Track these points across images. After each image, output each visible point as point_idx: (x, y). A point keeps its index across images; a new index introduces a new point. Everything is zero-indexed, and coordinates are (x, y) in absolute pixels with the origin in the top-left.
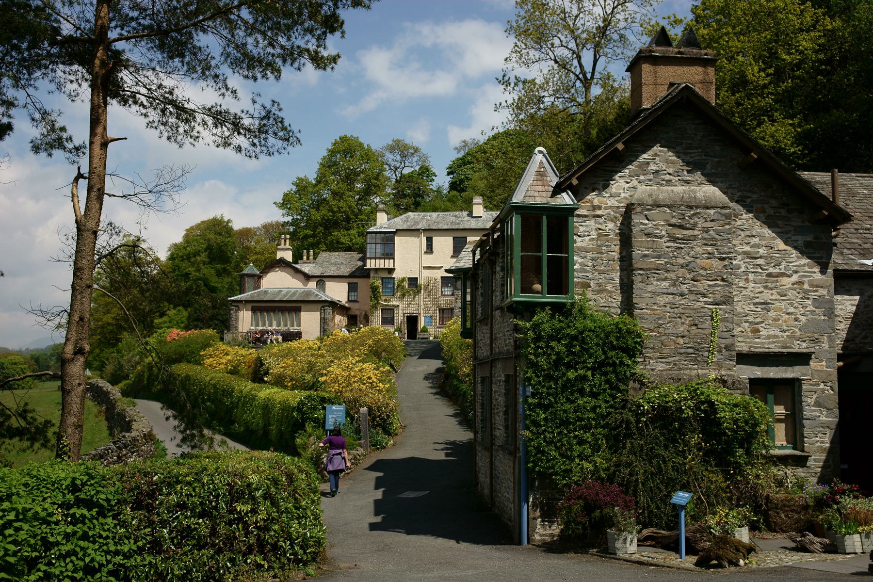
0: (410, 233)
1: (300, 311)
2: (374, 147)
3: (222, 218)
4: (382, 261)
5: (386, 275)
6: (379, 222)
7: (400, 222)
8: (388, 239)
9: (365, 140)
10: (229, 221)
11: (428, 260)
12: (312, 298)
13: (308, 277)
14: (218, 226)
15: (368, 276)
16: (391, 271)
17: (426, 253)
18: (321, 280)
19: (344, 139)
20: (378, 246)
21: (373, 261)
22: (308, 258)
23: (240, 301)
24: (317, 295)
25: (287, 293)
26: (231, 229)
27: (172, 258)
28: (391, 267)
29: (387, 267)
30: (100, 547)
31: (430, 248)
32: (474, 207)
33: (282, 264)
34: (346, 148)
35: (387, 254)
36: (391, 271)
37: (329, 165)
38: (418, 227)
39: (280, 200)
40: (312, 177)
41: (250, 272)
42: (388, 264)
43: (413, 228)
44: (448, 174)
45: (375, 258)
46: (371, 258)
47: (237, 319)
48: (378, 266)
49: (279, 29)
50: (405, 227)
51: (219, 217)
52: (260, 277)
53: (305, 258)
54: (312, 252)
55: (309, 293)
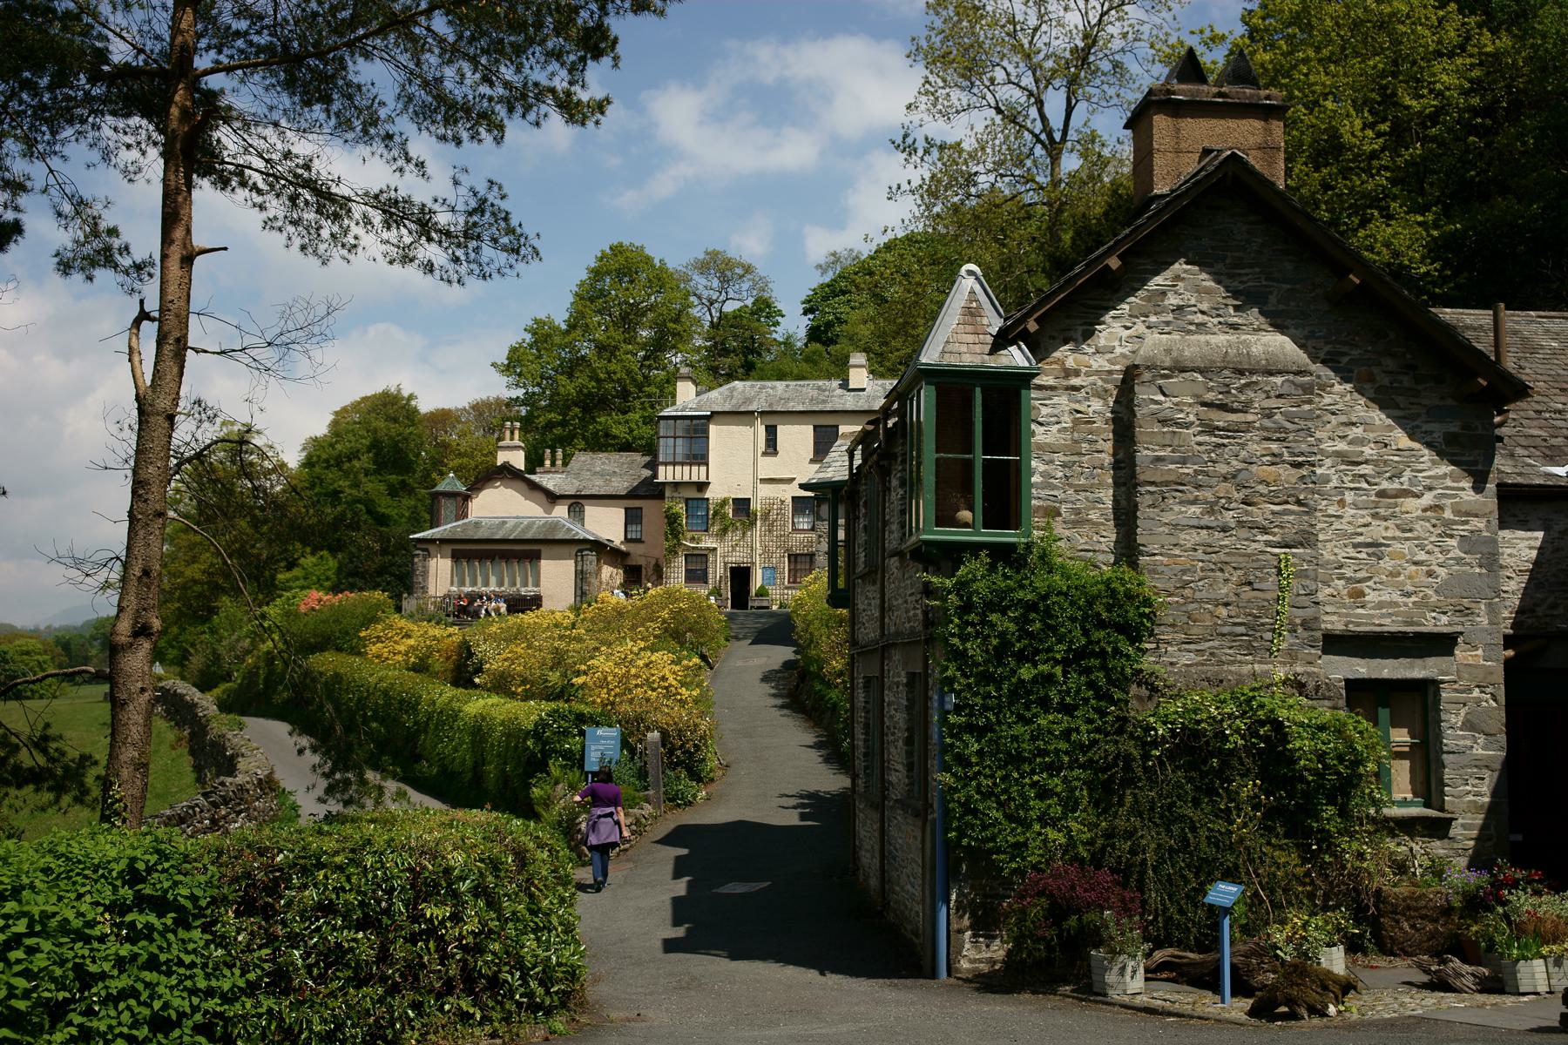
0: (736, 418)
1: (539, 558)
2: (672, 265)
4: (686, 468)
5: (694, 494)
6: (680, 399)
7: (718, 398)
8: (697, 429)
9: (656, 252)
10: (411, 397)
11: (768, 467)
12: (560, 536)
13: (552, 498)
14: (392, 407)
15: (661, 496)
16: (702, 486)
17: (765, 454)
18: (577, 502)
19: (617, 250)
20: (680, 441)
21: (670, 468)
22: (553, 464)
23: (432, 541)
24: (569, 530)
26: (416, 411)
27: (308, 463)
28: (703, 479)
29: (695, 479)
31: (772, 446)
32: (852, 371)
33: (507, 474)
34: (622, 266)
35: (695, 457)
36: (702, 486)
37: (590, 296)
38: (751, 408)
39: (502, 359)
40: (560, 318)
41: (448, 489)
42: (696, 474)
43: (742, 409)
44: (805, 313)
45: (674, 464)
46: (666, 464)
47: (425, 573)
48: (678, 478)
50: (727, 408)
51: (393, 390)
52: (467, 498)
53: (548, 463)
54: (560, 453)
55: (555, 526)
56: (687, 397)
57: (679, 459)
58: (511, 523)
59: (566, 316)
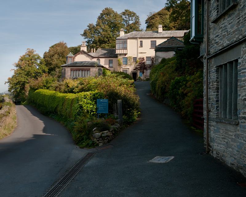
3: (63, 42)
4: (122, 50)
6: (121, 36)
7: (129, 35)
8: (124, 41)
10: (65, 43)
15: (117, 57)
17: (140, 47)
19: (106, 9)
22: (93, 52)
28: (126, 53)
29: (124, 53)
30: (186, 86)
32: (159, 28)
33: (84, 52)
34: (107, 12)
35: (124, 48)
36: (125, 54)
37: (101, 18)
38: (137, 37)
40: (95, 23)
41: (70, 56)
43: (135, 37)
44: (146, 23)
45: (120, 50)
48: (121, 53)
50: (131, 37)
51: (62, 42)
53: (92, 51)
54: (95, 49)
56: (122, 34)
59: (96, 23)
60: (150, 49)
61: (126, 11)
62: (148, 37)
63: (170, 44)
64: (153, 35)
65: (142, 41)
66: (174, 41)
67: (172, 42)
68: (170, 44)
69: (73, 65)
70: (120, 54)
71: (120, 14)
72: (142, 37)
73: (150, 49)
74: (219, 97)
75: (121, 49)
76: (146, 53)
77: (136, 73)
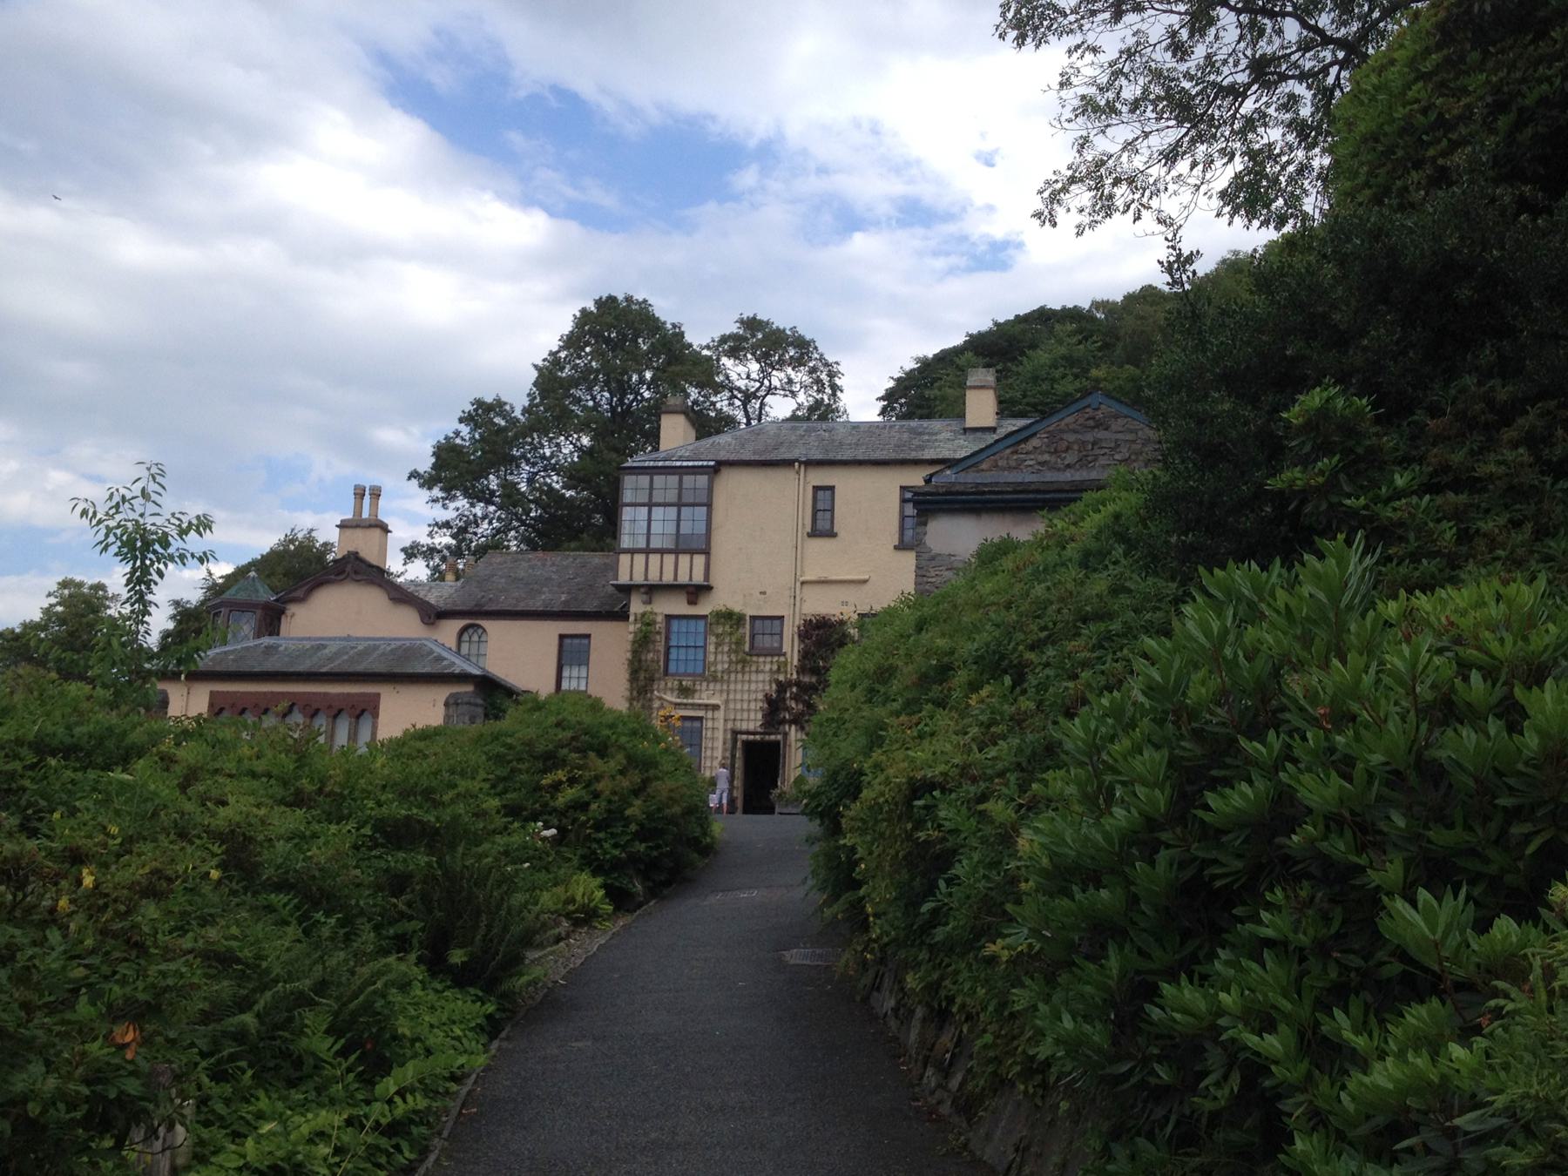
9: (666, 310)
19: (607, 305)
21: (640, 559)
24: (440, 659)
25: (337, 654)
28: (698, 578)
29: (683, 578)
31: (822, 526)
32: (968, 393)
36: (696, 592)
38: (787, 456)
39: (426, 464)
42: (689, 569)
45: (647, 551)
46: (632, 552)
48: (654, 577)
49: (656, 736)
57: (655, 544)
58: (332, 648)
60: (414, 475)
61: (752, 324)
62: (878, 455)
63: (1070, 458)
64: (922, 448)
65: (832, 488)
66: (1099, 425)
67: (1089, 437)
68: (1070, 458)
69: (244, 668)
70: (652, 590)
71: (708, 347)
72: (831, 456)
73: (414, 475)
74: (743, 637)
75: (656, 551)
76: (865, 581)
77: (746, 744)
